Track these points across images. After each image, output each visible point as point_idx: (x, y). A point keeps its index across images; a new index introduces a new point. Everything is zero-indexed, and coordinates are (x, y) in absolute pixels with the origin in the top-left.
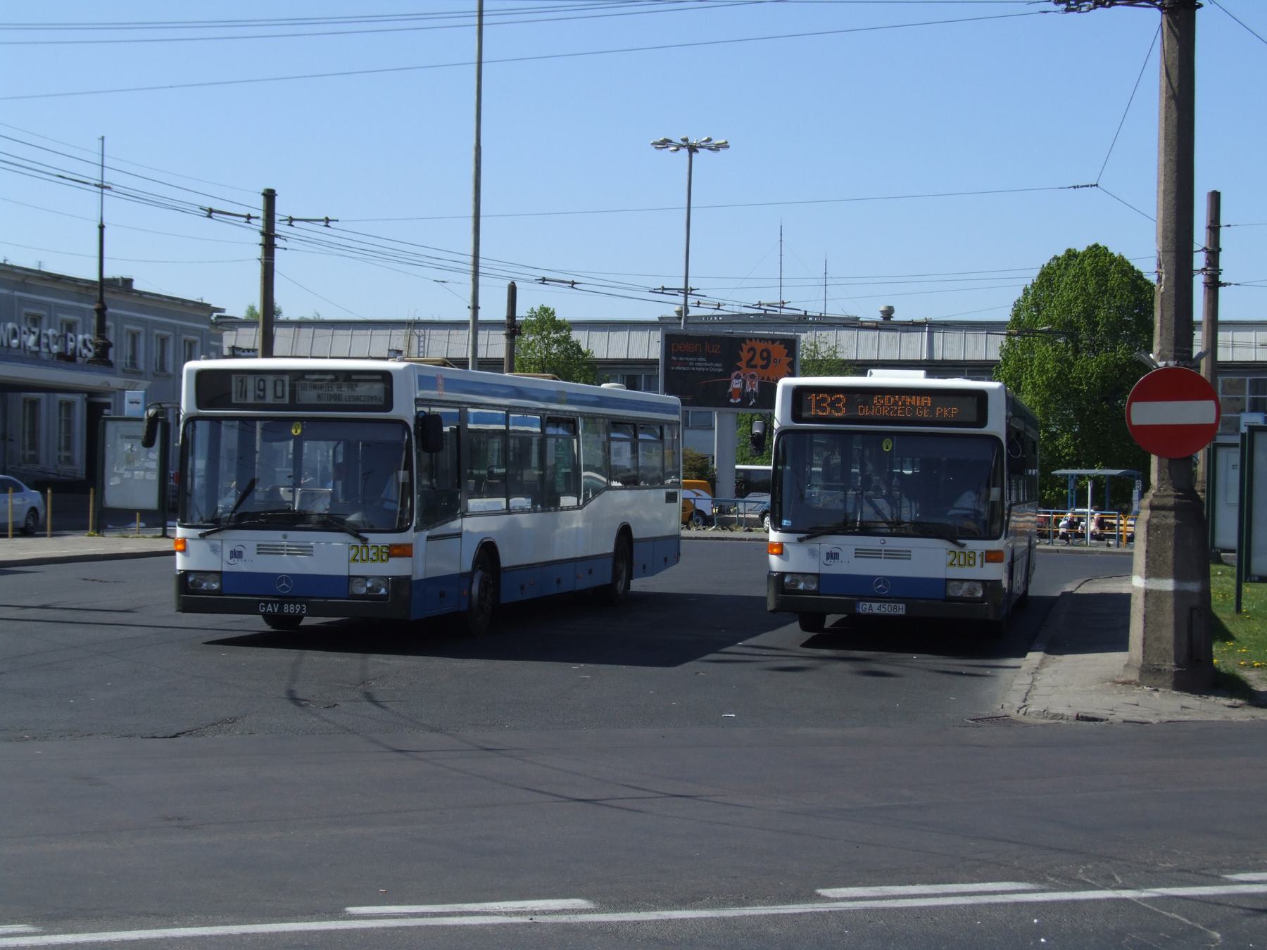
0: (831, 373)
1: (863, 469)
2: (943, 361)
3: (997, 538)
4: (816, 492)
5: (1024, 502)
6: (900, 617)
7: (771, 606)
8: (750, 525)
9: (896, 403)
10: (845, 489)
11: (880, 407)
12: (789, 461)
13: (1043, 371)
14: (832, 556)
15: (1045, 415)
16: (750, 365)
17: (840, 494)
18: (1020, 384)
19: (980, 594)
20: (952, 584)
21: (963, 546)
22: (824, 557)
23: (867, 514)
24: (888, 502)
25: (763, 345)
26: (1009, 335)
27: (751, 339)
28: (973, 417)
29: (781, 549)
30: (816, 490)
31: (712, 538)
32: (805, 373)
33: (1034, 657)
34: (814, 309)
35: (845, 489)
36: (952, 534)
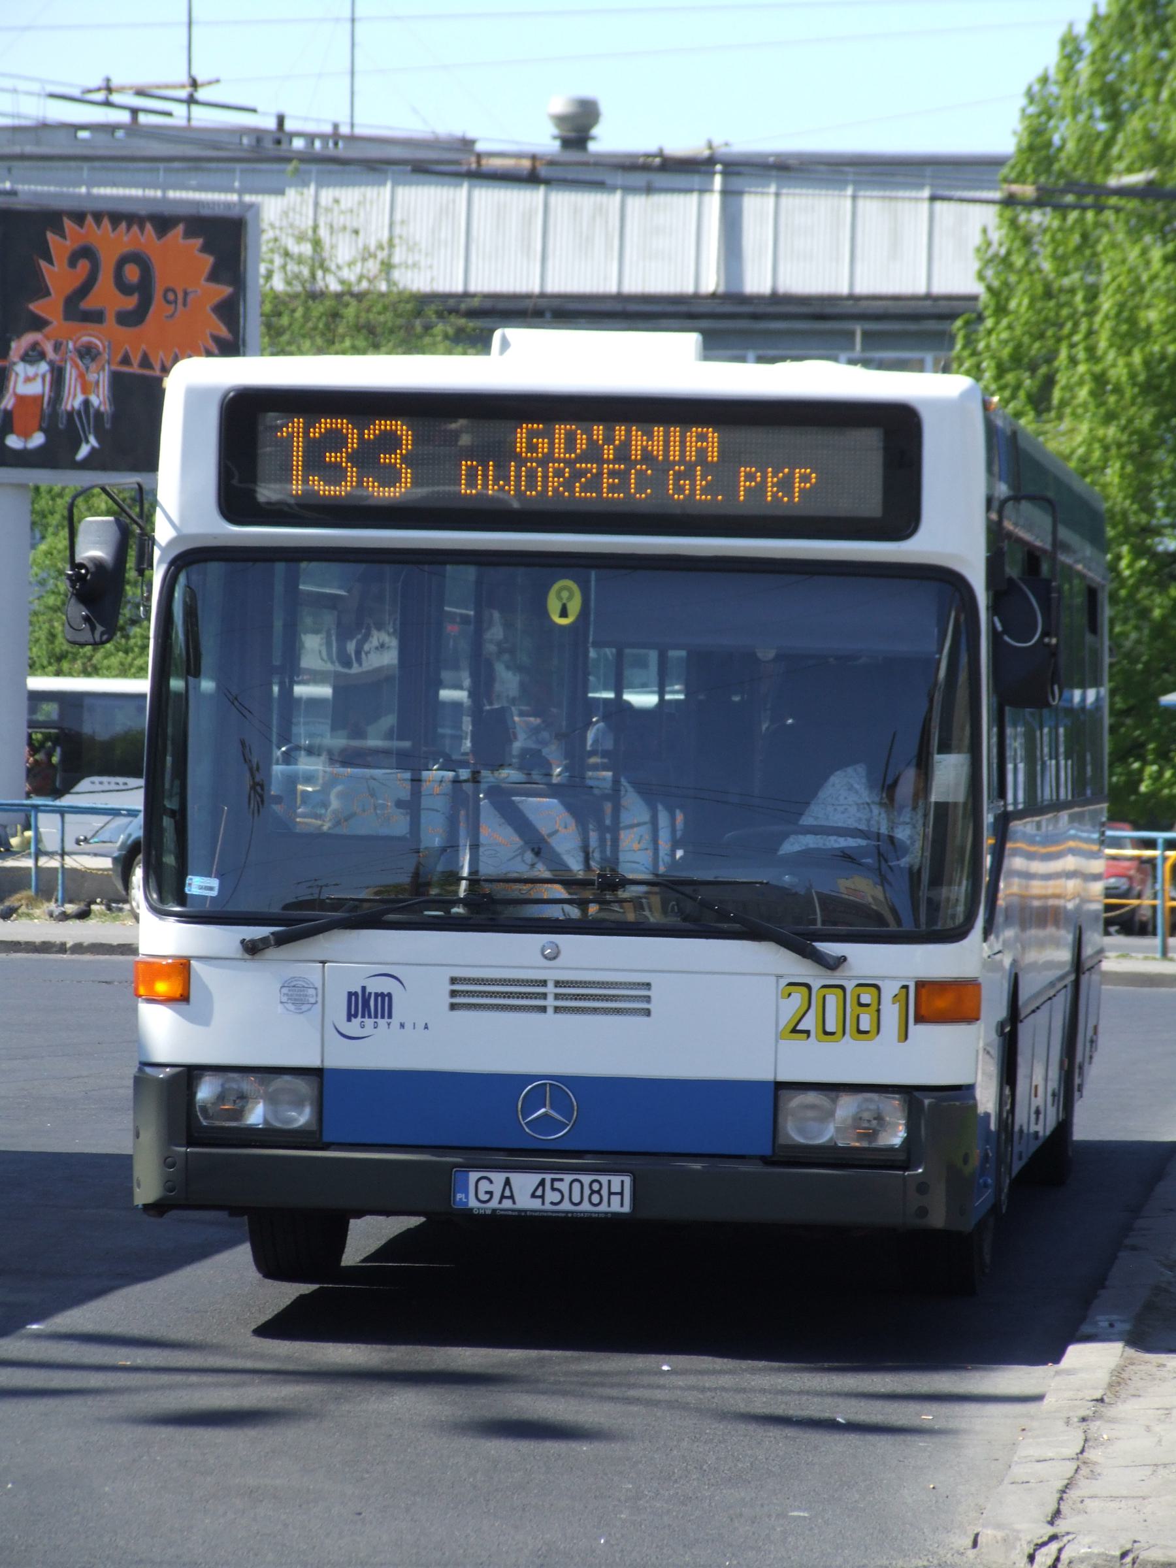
0: (371, 338)
1: (482, 688)
2: (775, 298)
3: (957, 934)
4: (315, 783)
5: (1057, 806)
6: (613, 1221)
7: (147, 1187)
8: (85, 895)
9: (593, 454)
10: (412, 763)
11: (546, 465)
12: (207, 661)
13: (1131, 333)
14: (367, 1005)
15: (1141, 493)
16: (78, 309)
17: (397, 781)
18: (1049, 382)
19: (896, 1136)
20: (799, 1100)
21: (835, 964)
22: (338, 1007)
23: (496, 850)
24: (570, 808)
25: (122, 240)
26: (1010, 201)
27: (79, 217)
28: (869, 501)
29: (181, 983)
30: (306, 765)
31: (45, 947)
32: (279, 341)
33: (1091, 1361)
34: (312, 111)
35: (412, 763)
36: (797, 923)
